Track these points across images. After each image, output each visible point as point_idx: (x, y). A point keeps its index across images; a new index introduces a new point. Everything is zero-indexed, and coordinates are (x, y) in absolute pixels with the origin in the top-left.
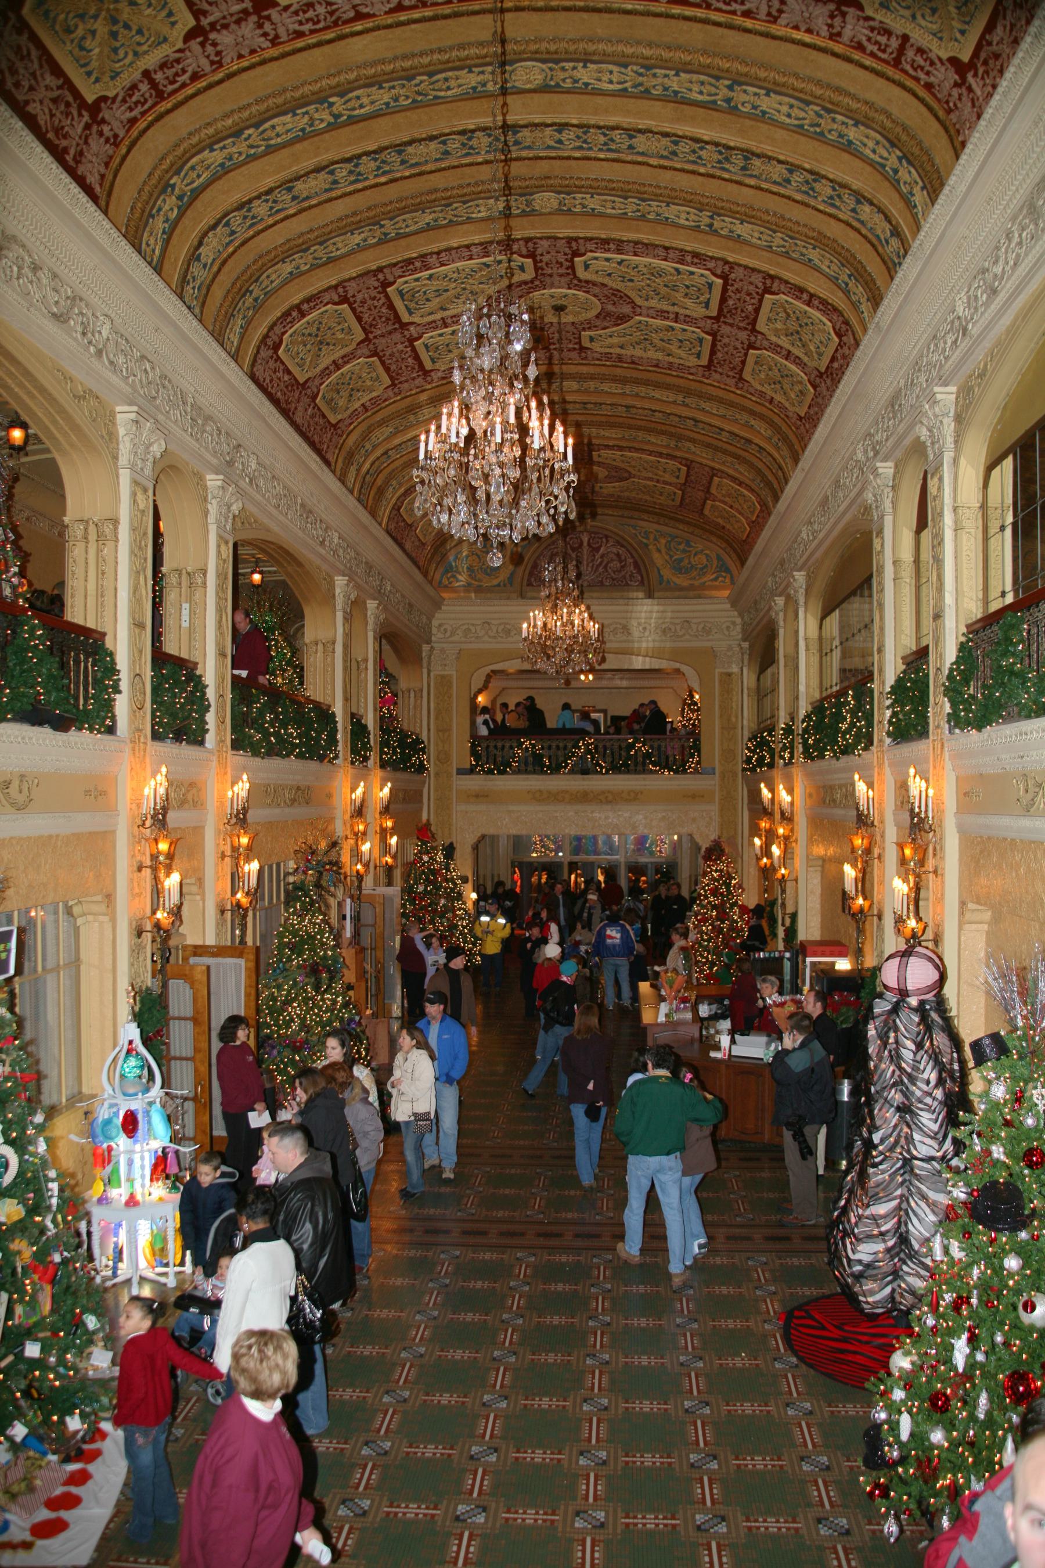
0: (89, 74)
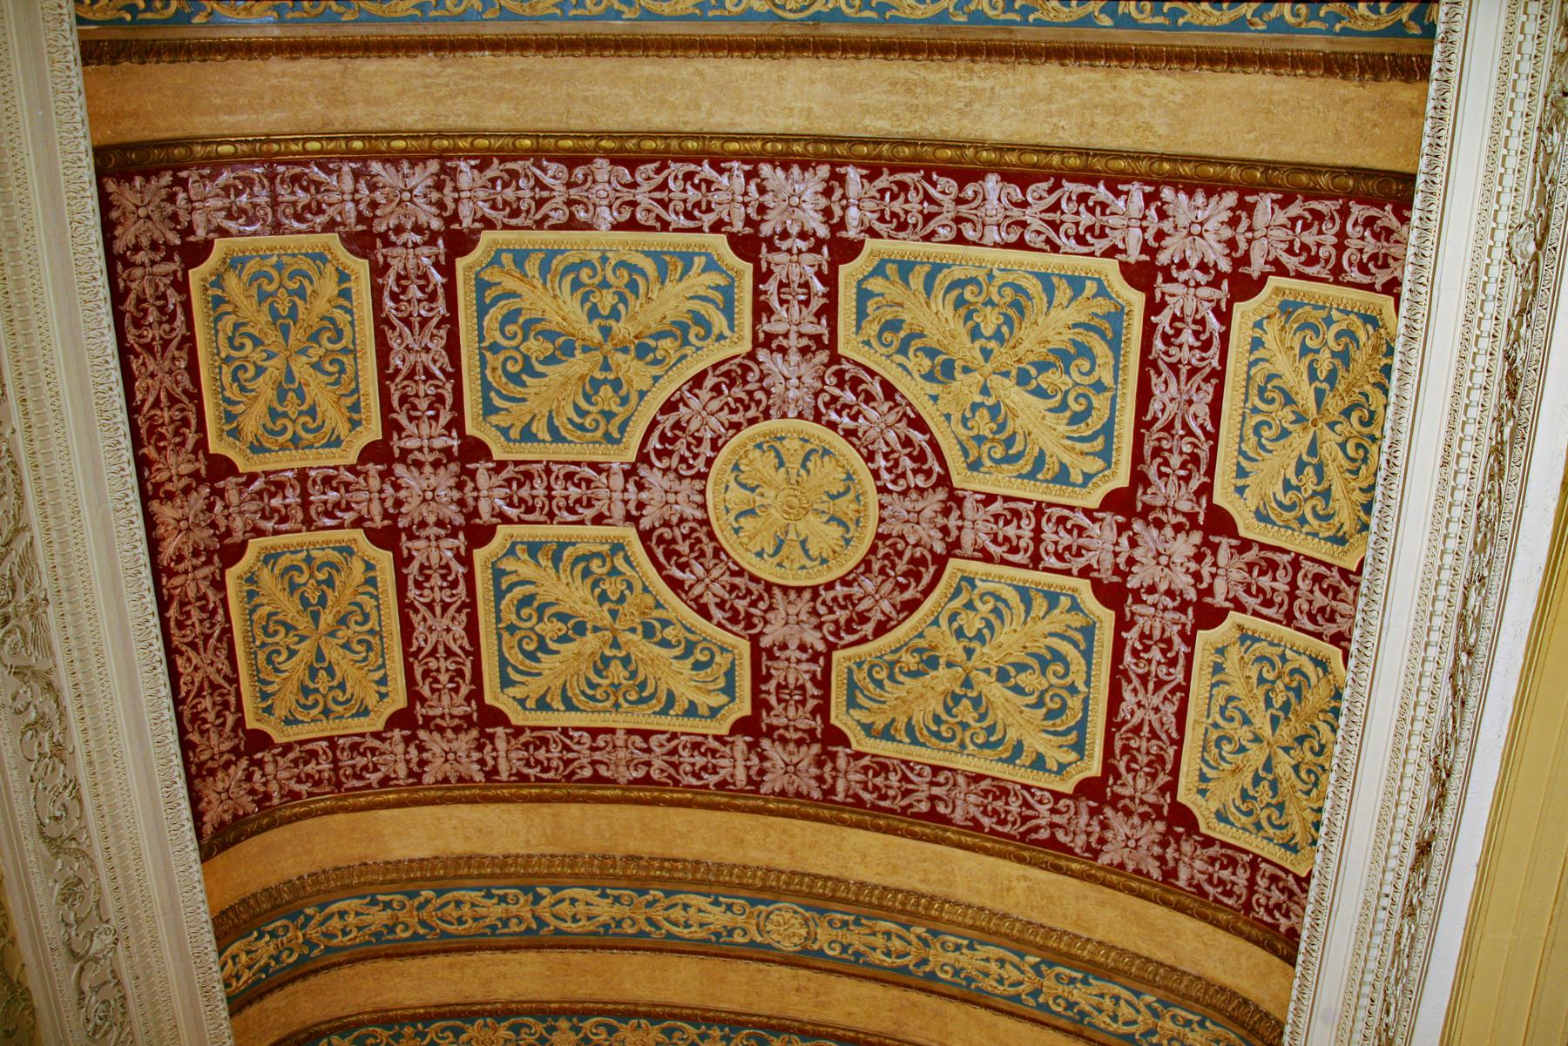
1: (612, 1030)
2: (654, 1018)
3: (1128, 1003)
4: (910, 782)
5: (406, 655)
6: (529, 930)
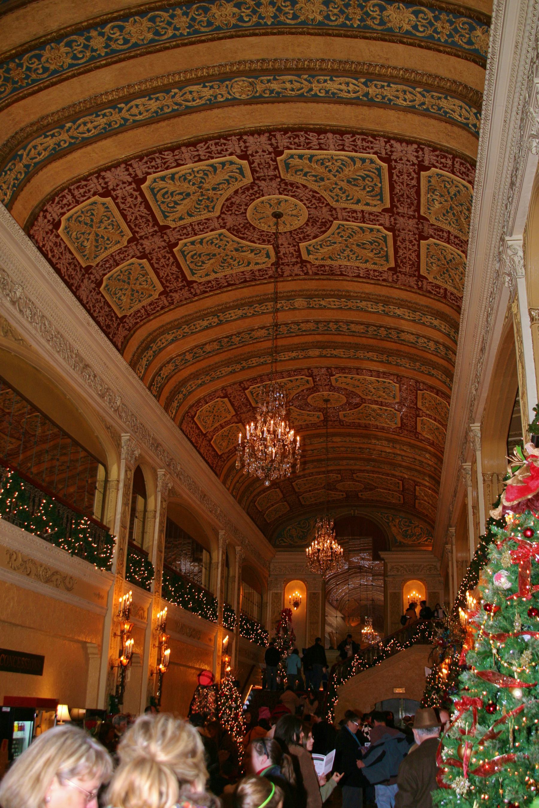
0: (85, 256)
1: (121, 29)
2: (142, 14)
3: (410, 93)
5: (127, 223)
6: (121, 125)
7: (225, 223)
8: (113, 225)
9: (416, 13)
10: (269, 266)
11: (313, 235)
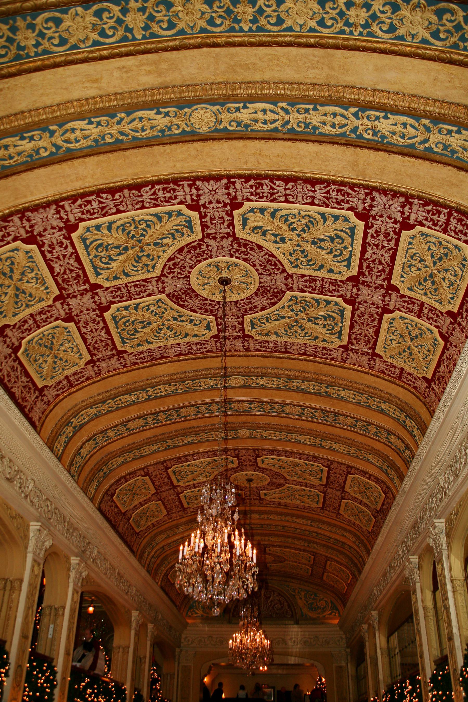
4: (274, 189)
5: (53, 277)
6: (52, 154)
7: (164, 288)
8: (37, 279)
9: (440, 13)
10: (208, 339)
11: (260, 306)
